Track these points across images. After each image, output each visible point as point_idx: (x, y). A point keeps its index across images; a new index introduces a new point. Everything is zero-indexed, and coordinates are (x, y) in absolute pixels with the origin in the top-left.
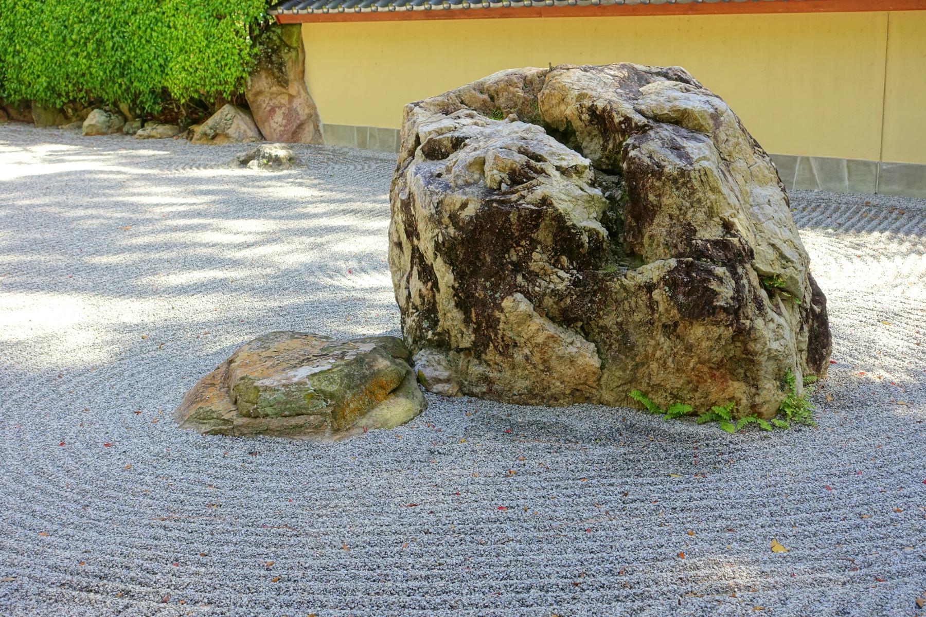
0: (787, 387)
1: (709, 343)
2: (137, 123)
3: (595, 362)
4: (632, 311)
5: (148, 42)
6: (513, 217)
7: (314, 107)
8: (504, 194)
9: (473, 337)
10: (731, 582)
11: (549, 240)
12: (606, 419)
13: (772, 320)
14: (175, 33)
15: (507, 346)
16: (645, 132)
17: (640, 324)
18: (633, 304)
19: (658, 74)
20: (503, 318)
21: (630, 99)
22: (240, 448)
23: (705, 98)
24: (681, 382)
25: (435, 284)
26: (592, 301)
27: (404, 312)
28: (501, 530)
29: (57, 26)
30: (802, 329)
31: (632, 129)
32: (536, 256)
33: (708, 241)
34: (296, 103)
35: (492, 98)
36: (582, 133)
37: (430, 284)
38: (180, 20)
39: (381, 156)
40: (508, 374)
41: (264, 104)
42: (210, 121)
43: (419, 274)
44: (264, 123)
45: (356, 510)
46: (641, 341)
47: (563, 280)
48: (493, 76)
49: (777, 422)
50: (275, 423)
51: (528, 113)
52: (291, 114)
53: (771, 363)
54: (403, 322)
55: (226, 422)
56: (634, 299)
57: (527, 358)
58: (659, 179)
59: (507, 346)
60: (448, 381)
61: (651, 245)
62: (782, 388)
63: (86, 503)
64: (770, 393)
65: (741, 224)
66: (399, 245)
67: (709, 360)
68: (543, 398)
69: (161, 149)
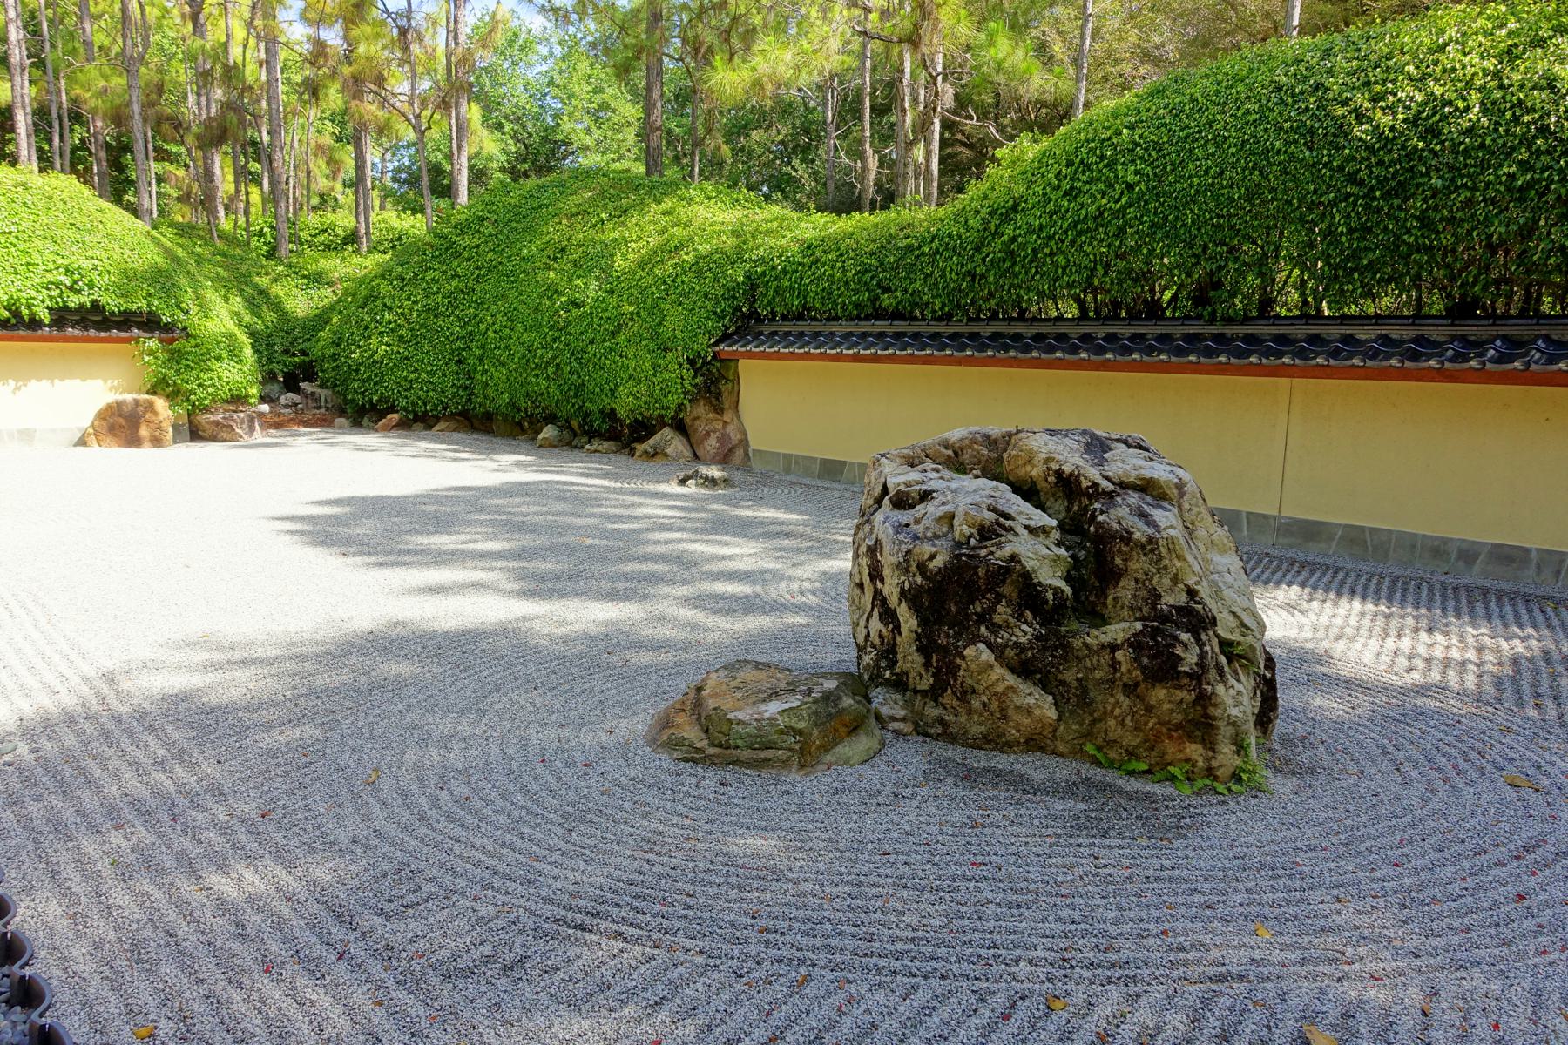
0: (1242, 752)
1: (1169, 706)
2: (585, 439)
3: (1052, 714)
4: (1093, 669)
5: (602, 368)
6: (981, 572)
7: (745, 434)
8: (974, 548)
9: (932, 680)
10: (1223, 969)
11: (1014, 595)
12: (1063, 770)
13: (1233, 687)
14: (626, 362)
15: (965, 692)
16: (1112, 497)
17: (1099, 682)
18: (1095, 662)
19: (1118, 440)
20: (964, 666)
21: (1096, 464)
22: (711, 777)
23: (1169, 468)
24: (1138, 740)
25: (897, 628)
26: (1052, 656)
27: (861, 649)
28: (977, 889)
29: (522, 350)
30: (1255, 694)
31: (1099, 494)
32: (1000, 609)
33: (1173, 606)
34: (730, 429)
35: (956, 454)
36: (1046, 493)
37: (891, 626)
38: (631, 352)
39: (805, 481)
40: (963, 719)
41: (701, 427)
42: (651, 441)
43: (880, 615)
44: (699, 444)
45: (831, 855)
46: (1100, 698)
47: (1025, 633)
48: (956, 434)
49: (1235, 787)
50: (745, 754)
51: (992, 471)
52: (723, 439)
53: (1230, 728)
54: (860, 658)
55: (698, 750)
56: (1096, 658)
57: (984, 705)
58: (1127, 544)
59: (965, 692)
60: (903, 720)
61: (1114, 606)
62: (1238, 753)
63: (570, 827)
64: (1227, 756)
65: (1204, 591)
66: (861, 586)
67: (1169, 722)
68: (997, 744)
69: (607, 464)
